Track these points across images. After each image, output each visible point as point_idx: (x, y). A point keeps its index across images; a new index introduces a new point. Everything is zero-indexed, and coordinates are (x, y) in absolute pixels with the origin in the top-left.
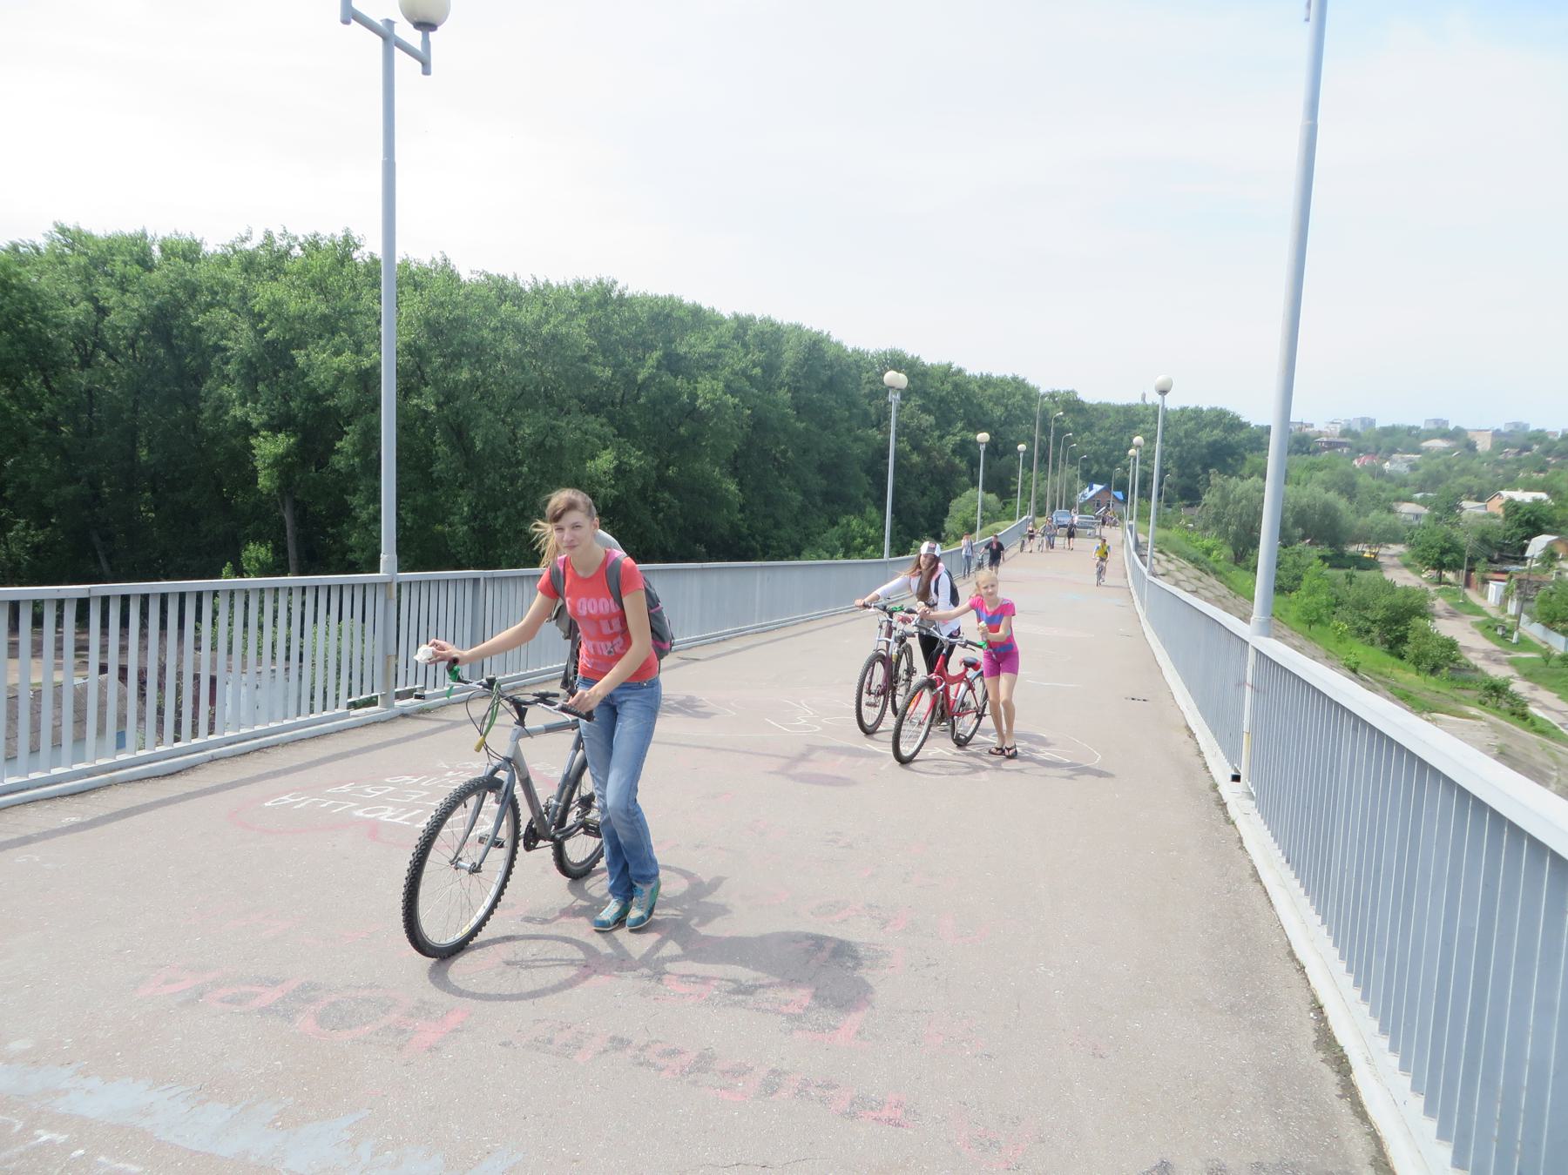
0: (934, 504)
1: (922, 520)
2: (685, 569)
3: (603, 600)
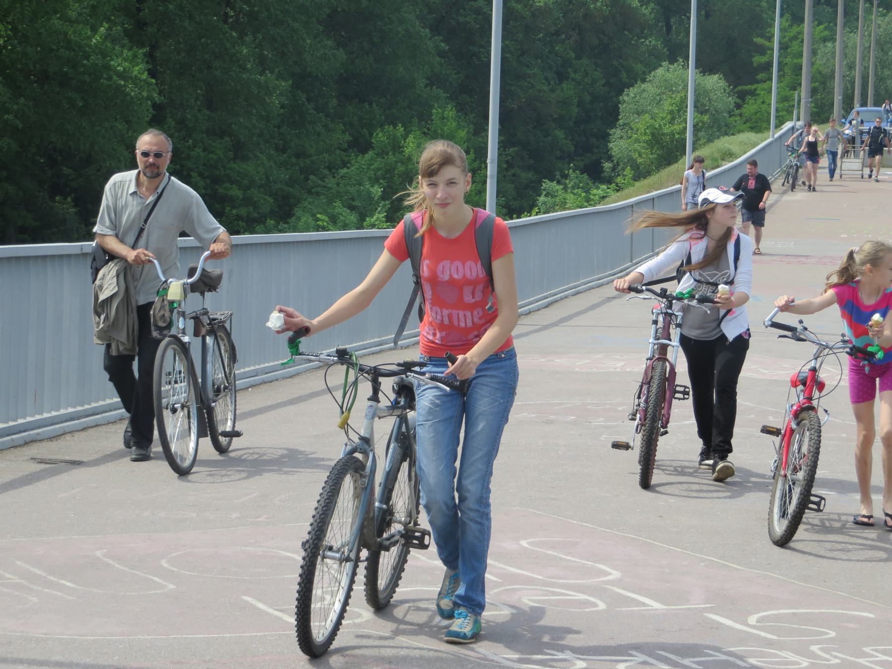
0: (588, 98)
1: (560, 134)
2: (44, 257)
3: (470, 263)
